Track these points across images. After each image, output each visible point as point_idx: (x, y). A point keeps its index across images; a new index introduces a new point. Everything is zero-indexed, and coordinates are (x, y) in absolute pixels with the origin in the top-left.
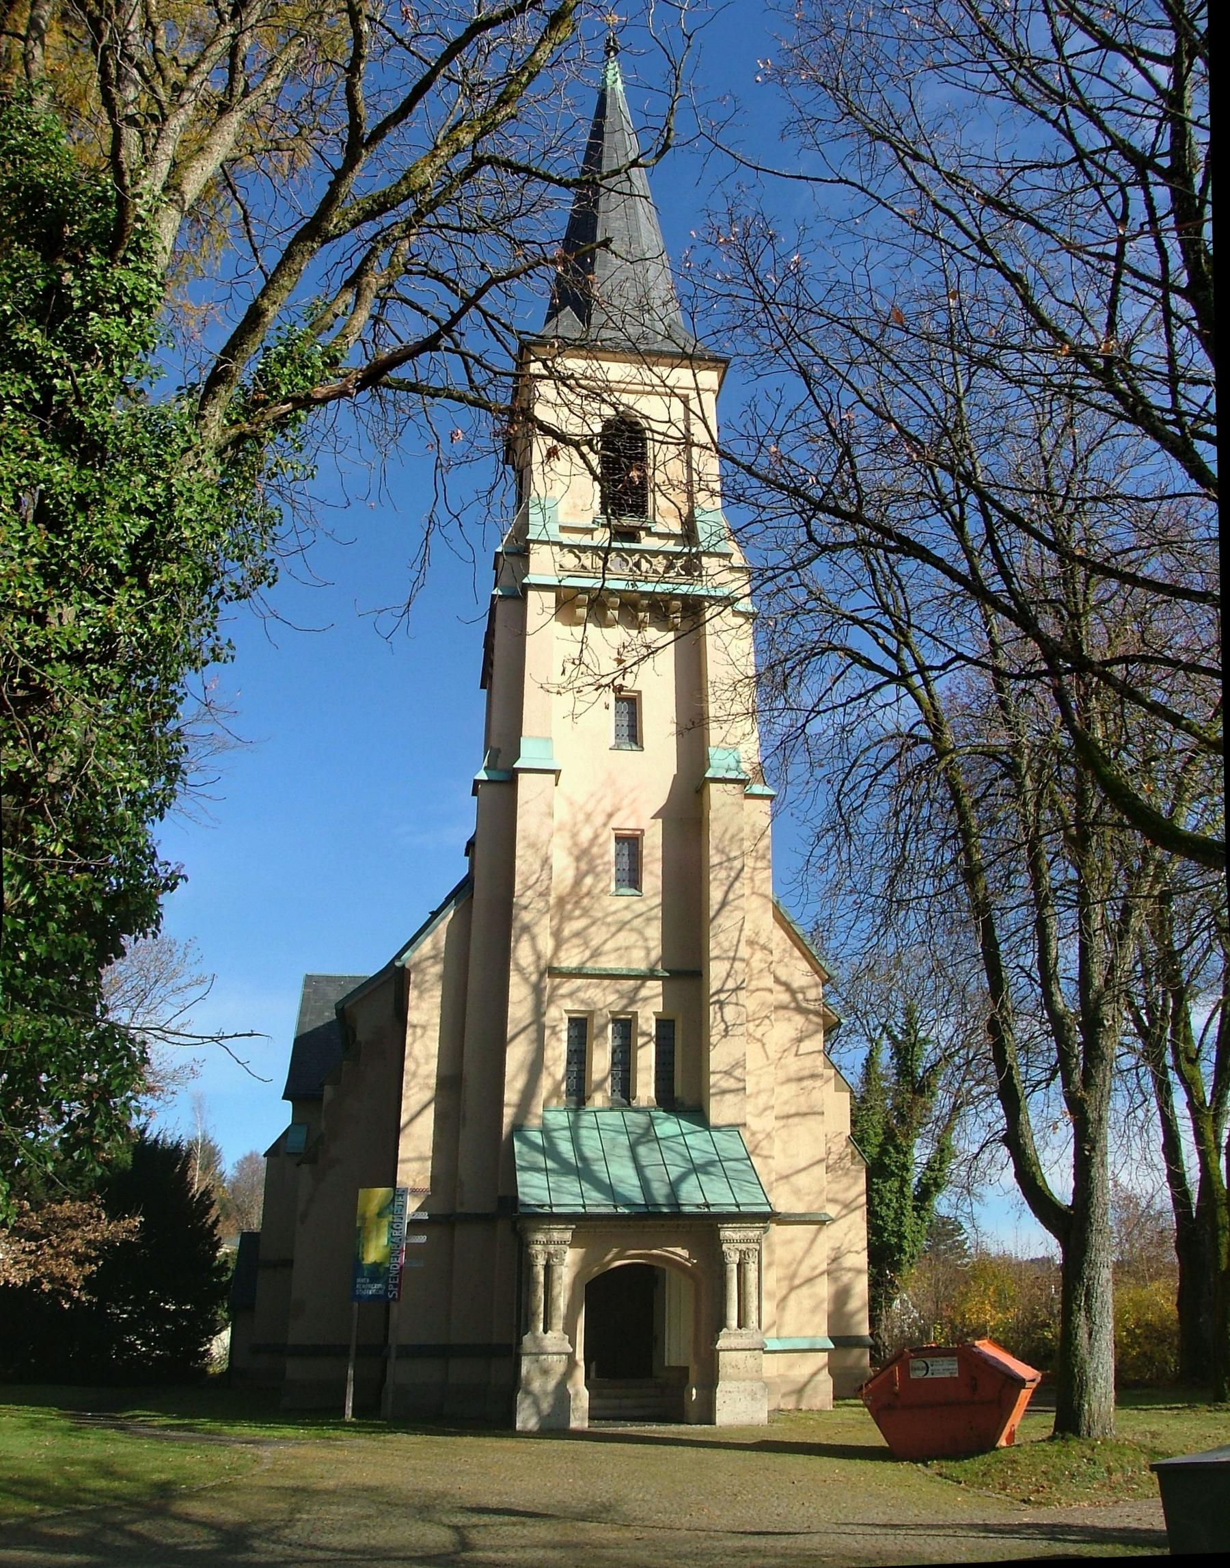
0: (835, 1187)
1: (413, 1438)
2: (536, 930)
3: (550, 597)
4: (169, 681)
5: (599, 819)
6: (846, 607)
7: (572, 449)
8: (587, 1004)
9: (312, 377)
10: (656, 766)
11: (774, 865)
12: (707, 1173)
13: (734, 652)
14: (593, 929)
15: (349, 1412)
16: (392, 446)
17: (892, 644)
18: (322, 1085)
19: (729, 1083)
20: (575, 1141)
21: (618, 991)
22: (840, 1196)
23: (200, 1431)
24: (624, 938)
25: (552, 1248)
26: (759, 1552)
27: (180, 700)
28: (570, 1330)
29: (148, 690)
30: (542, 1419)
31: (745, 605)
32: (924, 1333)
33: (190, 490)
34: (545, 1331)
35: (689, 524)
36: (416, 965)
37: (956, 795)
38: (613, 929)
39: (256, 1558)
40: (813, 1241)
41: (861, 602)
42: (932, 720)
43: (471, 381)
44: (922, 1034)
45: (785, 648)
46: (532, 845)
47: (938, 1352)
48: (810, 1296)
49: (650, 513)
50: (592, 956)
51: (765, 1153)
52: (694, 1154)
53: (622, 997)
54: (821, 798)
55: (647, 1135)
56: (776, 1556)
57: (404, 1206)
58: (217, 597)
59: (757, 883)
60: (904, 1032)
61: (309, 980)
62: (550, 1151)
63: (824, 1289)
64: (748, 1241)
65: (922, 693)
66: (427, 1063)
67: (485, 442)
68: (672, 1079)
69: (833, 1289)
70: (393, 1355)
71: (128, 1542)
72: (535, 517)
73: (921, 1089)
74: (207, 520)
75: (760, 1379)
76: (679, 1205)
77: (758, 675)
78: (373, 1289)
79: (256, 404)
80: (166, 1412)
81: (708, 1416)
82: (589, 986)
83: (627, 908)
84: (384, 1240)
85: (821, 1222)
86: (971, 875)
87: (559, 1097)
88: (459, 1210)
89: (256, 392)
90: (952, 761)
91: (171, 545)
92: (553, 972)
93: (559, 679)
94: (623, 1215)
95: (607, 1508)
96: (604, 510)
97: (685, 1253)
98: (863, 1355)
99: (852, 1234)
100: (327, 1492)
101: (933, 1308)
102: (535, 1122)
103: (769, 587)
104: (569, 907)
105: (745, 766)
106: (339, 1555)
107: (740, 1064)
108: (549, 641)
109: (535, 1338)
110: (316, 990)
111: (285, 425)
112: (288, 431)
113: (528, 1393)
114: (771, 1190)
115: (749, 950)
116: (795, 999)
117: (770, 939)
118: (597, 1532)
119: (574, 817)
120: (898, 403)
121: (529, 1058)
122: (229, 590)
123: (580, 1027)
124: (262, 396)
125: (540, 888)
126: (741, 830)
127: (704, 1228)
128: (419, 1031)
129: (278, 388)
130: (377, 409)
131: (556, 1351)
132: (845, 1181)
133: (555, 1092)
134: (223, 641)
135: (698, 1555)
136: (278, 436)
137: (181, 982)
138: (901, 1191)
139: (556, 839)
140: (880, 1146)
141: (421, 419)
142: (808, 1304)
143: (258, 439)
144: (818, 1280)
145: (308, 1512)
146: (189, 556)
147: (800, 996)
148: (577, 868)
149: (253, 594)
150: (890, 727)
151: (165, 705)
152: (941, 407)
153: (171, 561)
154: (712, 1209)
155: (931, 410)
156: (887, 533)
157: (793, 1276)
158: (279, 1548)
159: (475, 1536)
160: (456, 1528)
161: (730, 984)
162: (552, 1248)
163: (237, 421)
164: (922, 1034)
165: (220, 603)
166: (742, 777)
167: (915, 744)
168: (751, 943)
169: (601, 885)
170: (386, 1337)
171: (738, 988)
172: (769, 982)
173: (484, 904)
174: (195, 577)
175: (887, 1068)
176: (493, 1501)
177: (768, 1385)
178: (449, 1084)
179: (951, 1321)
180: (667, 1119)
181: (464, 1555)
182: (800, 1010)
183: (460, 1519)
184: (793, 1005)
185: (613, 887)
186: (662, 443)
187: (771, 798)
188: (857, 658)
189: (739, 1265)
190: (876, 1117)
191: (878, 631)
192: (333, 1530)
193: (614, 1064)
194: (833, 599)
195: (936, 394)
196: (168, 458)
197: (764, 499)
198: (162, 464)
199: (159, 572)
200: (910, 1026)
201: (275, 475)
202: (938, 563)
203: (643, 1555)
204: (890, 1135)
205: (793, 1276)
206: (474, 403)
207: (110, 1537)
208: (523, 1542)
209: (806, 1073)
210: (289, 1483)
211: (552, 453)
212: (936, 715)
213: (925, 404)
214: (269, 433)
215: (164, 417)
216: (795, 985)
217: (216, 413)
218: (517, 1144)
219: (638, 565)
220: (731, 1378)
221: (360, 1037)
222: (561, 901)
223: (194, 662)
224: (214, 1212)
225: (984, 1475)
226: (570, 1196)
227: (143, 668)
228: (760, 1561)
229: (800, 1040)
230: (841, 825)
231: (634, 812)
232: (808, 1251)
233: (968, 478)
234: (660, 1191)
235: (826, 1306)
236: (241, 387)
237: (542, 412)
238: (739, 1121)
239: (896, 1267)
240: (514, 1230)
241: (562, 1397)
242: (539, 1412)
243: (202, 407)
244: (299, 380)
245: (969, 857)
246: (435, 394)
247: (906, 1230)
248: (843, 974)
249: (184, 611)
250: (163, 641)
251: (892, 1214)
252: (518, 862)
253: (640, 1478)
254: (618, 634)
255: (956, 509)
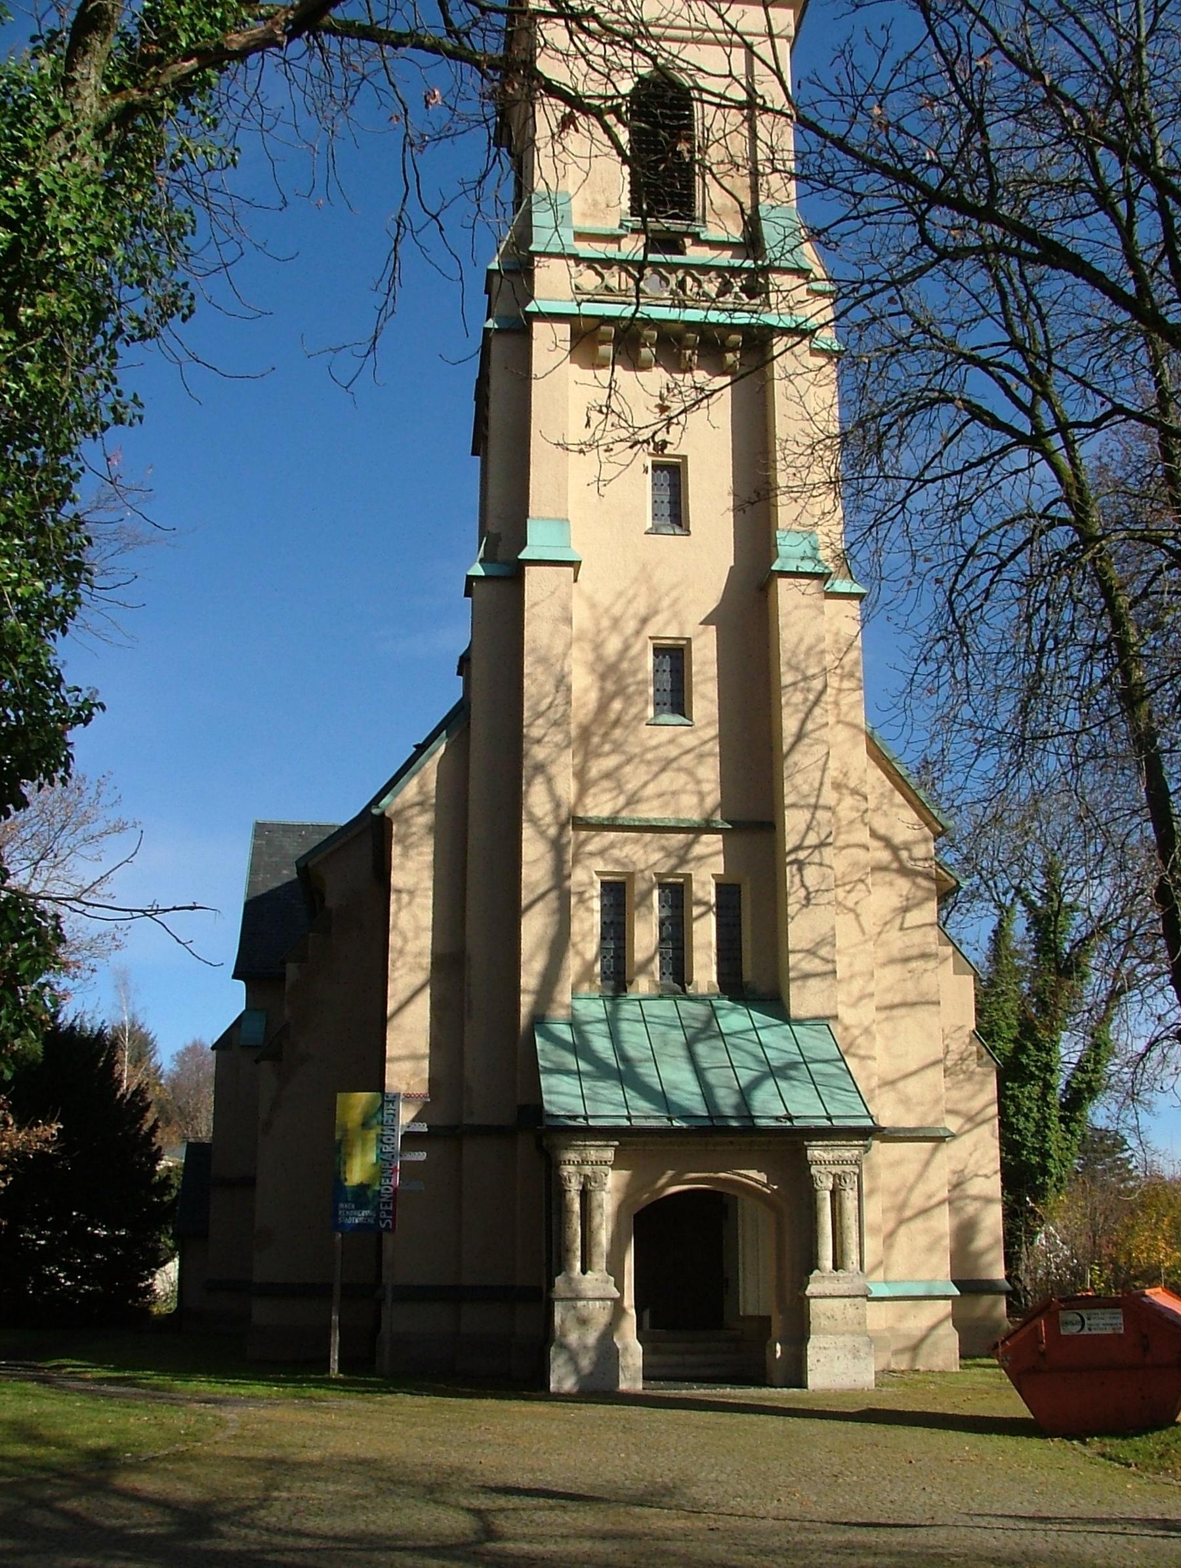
0: (955, 1094)
1: (418, 1400)
2: (553, 770)
3: (564, 330)
4: (57, 452)
5: (631, 626)
6: (965, 343)
7: (593, 120)
8: (624, 865)
9: (223, 20)
10: (706, 556)
11: (867, 685)
12: (788, 1078)
13: (812, 405)
14: (628, 769)
15: (334, 1366)
16: (341, 120)
17: (1025, 394)
18: (283, 963)
19: (815, 965)
20: (614, 1036)
21: (663, 848)
22: (962, 1107)
23: (144, 1387)
24: (667, 781)
25: (588, 1170)
26: (871, 1550)
27: (75, 477)
28: (615, 1269)
29: (31, 466)
30: (582, 1379)
31: (826, 338)
32: (1078, 1274)
33: (64, 188)
34: (584, 1271)
35: (752, 224)
36: (399, 813)
37: (1107, 592)
38: (655, 768)
39: (226, 1545)
40: (927, 1164)
41: (986, 335)
42: (1076, 498)
43: (448, 22)
44: (1068, 899)
45: (880, 398)
46: (543, 660)
47: (1097, 1303)
48: (927, 1231)
49: (698, 213)
50: (628, 804)
51: (862, 1052)
52: (770, 1054)
53: (669, 855)
54: (927, 598)
55: (708, 1030)
56: (891, 1554)
57: (395, 1115)
58: (114, 337)
59: (844, 709)
60: (1044, 896)
61: (261, 829)
62: (582, 1049)
63: (944, 1222)
64: (844, 1162)
65: (1062, 457)
66: (417, 937)
67: (471, 107)
68: (739, 959)
69: (956, 1221)
70: (389, 1296)
71: (59, 1523)
72: (541, 218)
73: (1069, 969)
74: (92, 230)
75: (865, 1333)
76: (752, 1117)
77: (844, 435)
78: (359, 1217)
79: (148, 60)
80: (100, 1363)
81: (798, 1379)
82: (625, 842)
83: (672, 741)
84: (372, 1157)
85: (939, 1139)
86: (1131, 698)
87: (592, 982)
88: (467, 1121)
89: (146, 42)
90: (1101, 550)
91: (46, 266)
92: (581, 824)
93: (586, 435)
94: (679, 1130)
95: (668, 1491)
96: (635, 210)
97: (763, 1177)
98: (995, 1305)
99: (980, 1155)
100: (312, 1464)
101: (1089, 1244)
102: (560, 1013)
103: (859, 314)
104: (596, 740)
105: (824, 554)
106: (330, 1544)
107: (829, 940)
108: (564, 391)
109: (570, 1280)
110: (269, 843)
111: (190, 91)
112: (195, 100)
113: (563, 1347)
114: (871, 1099)
115: (836, 795)
116: (897, 858)
117: (863, 781)
118: (658, 1520)
119: (597, 623)
120: (1054, 52)
121: (551, 932)
122: (129, 327)
123: (617, 896)
124: (154, 49)
125: (554, 715)
126: (821, 639)
127: (788, 1145)
128: (405, 897)
129: (175, 37)
130: (317, 65)
131: (599, 1296)
132: (969, 1088)
133: (586, 974)
134: (127, 397)
135: (793, 1551)
136: (181, 107)
137: (95, 828)
138: (1043, 1097)
139: (575, 652)
140: (1015, 1041)
141: (381, 80)
142: (922, 1241)
143: (153, 112)
144: (936, 1211)
145: (289, 1489)
146: (71, 281)
147: (904, 854)
148: (602, 689)
149: (162, 331)
150: (1021, 505)
151: (56, 484)
152: (1113, 57)
153: (47, 289)
154: (796, 1123)
155: (1097, 61)
156: (1030, 236)
157: (902, 1207)
158: (253, 1534)
159: (502, 1523)
160: (477, 1513)
161: (812, 839)
162: (588, 1170)
163: (121, 87)
164: (1068, 899)
165: (119, 346)
166: (819, 569)
167: (1051, 527)
168: (837, 786)
169: (633, 711)
170: (379, 1276)
171: (822, 844)
172: (863, 836)
173: (485, 735)
174: (82, 311)
175: (1024, 942)
176: (523, 1480)
177: (874, 1341)
178: (448, 966)
179: (1113, 1261)
180: (733, 1010)
181: (490, 1545)
182: (904, 871)
183: (482, 1502)
184: (895, 865)
185: (650, 711)
186: (719, 106)
187: (860, 597)
188: (977, 413)
189: (833, 1193)
190: (1009, 1005)
191: (1007, 376)
192: (320, 1512)
193: (662, 940)
194: (947, 331)
195: (1106, 38)
196: (30, 143)
197: (861, 184)
198: (21, 153)
199: (33, 305)
200: (1052, 891)
201: (181, 163)
202: (1096, 279)
203: (719, 1551)
204: (1027, 1028)
205: (902, 1207)
206: (452, 55)
207: (38, 1516)
208: (565, 1531)
209: (914, 952)
210: (260, 1452)
211: (567, 122)
212: (1080, 491)
213: (1091, 53)
214: (168, 103)
215: (18, 82)
216: (898, 839)
217: (90, 75)
218: (538, 1039)
219: (682, 284)
220: (825, 1332)
221: (331, 902)
222: (585, 733)
223: (88, 427)
224: (151, 1116)
225: (1161, 1456)
226: (611, 1105)
227: (21, 437)
228: (870, 1560)
229: (906, 910)
230: (956, 631)
231: (676, 615)
232: (920, 1176)
233: (1144, 163)
234: (726, 1100)
235: (947, 1242)
236: (123, 36)
237: (547, 66)
238: (828, 1013)
239: (1039, 1193)
240: (539, 1146)
241: (608, 1353)
242: (577, 1370)
243: (70, 67)
244: (203, 24)
245: (1127, 675)
246: (397, 41)
247: (1052, 1146)
248: (962, 824)
249: (71, 356)
250: (44, 398)
251: (1032, 1126)
252: (527, 682)
253: (710, 1453)
254: (657, 378)
255: (1122, 208)
